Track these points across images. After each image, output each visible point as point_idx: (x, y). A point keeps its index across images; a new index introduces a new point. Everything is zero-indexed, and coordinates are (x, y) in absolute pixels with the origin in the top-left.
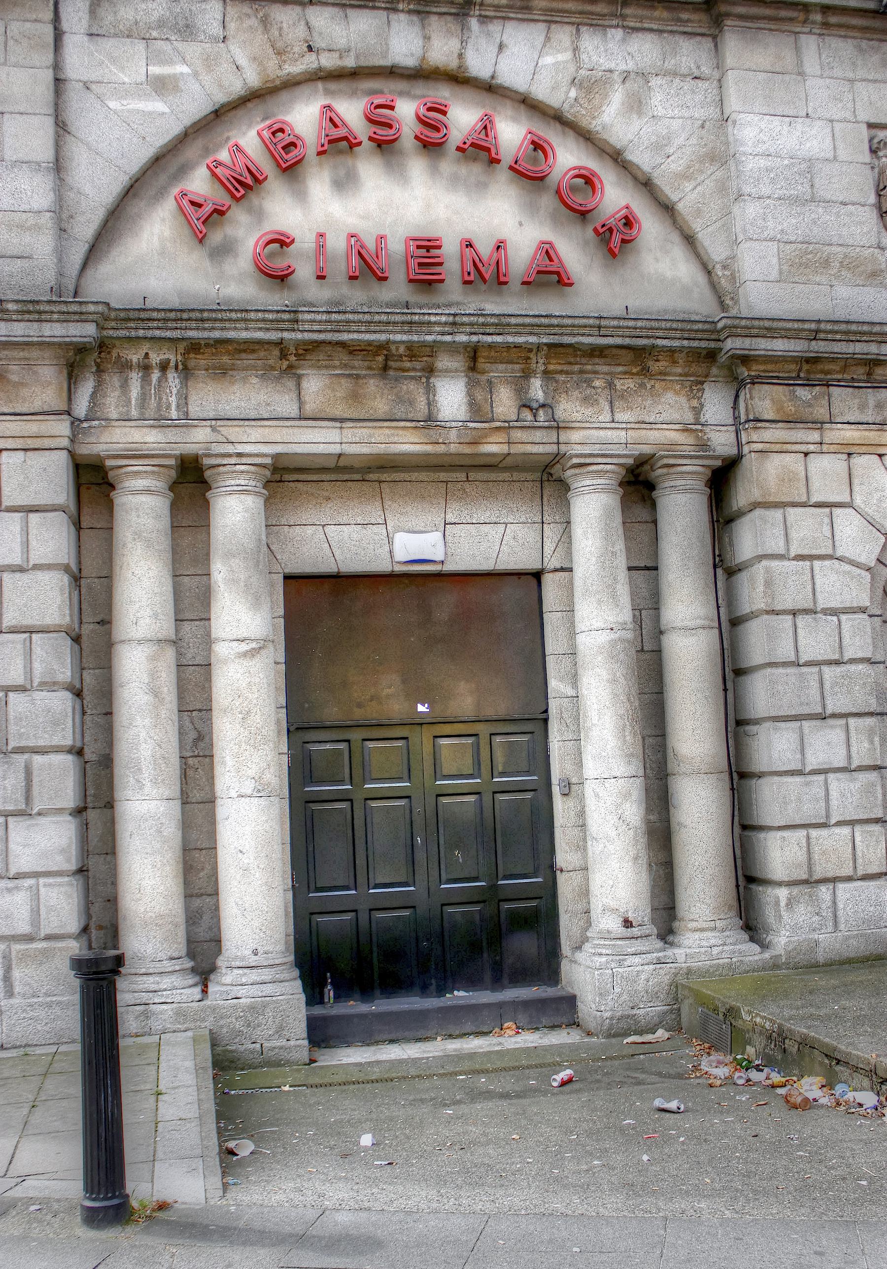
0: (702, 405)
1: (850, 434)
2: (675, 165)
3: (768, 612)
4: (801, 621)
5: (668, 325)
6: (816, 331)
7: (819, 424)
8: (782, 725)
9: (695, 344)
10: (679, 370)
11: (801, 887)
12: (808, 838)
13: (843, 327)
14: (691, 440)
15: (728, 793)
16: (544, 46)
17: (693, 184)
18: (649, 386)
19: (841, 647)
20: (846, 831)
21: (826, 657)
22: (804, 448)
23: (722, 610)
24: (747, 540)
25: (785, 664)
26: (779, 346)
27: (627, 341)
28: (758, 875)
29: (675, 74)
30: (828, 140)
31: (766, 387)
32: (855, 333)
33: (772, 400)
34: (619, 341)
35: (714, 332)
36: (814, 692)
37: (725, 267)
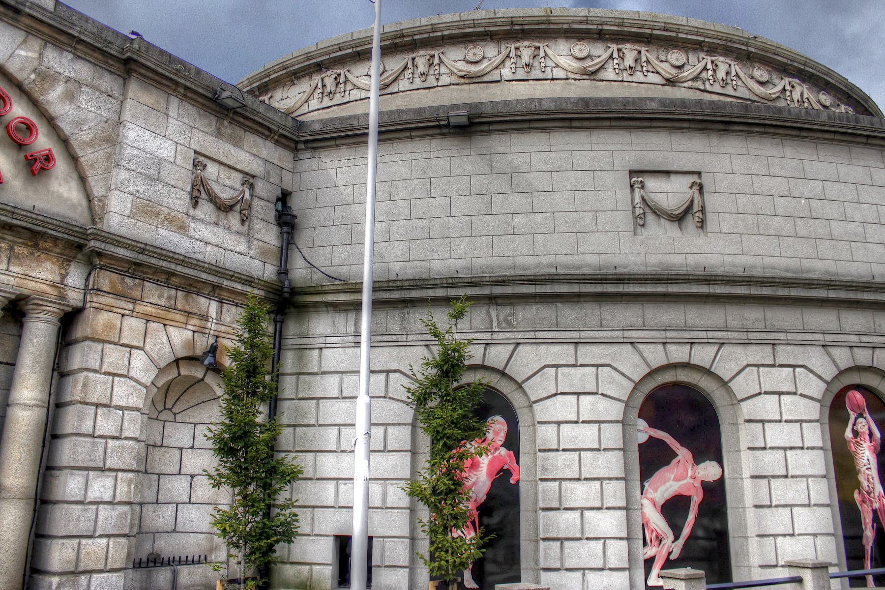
0: (67, 274)
1: (150, 309)
2: (85, 136)
3: (81, 403)
4: (100, 411)
5: (58, 223)
6: (144, 248)
7: (134, 301)
8: (77, 472)
9: (72, 238)
10: (58, 251)
11: (68, 576)
12: (79, 544)
13: (159, 251)
14: (55, 293)
15: (31, 512)
16: (21, 44)
17: (93, 150)
18: (36, 255)
19: (121, 429)
20: (104, 541)
21: (111, 434)
22: (122, 311)
23: (52, 397)
24: (78, 358)
25: (85, 435)
26: (121, 252)
27: (29, 226)
28: (42, 568)
29: (97, 89)
30: (173, 152)
31: (108, 273)
32: (165, 256)
33: (110, 281)
34: (24, 224)
35: (84, 234)
36: (100, 454)
37: (100, 200)
